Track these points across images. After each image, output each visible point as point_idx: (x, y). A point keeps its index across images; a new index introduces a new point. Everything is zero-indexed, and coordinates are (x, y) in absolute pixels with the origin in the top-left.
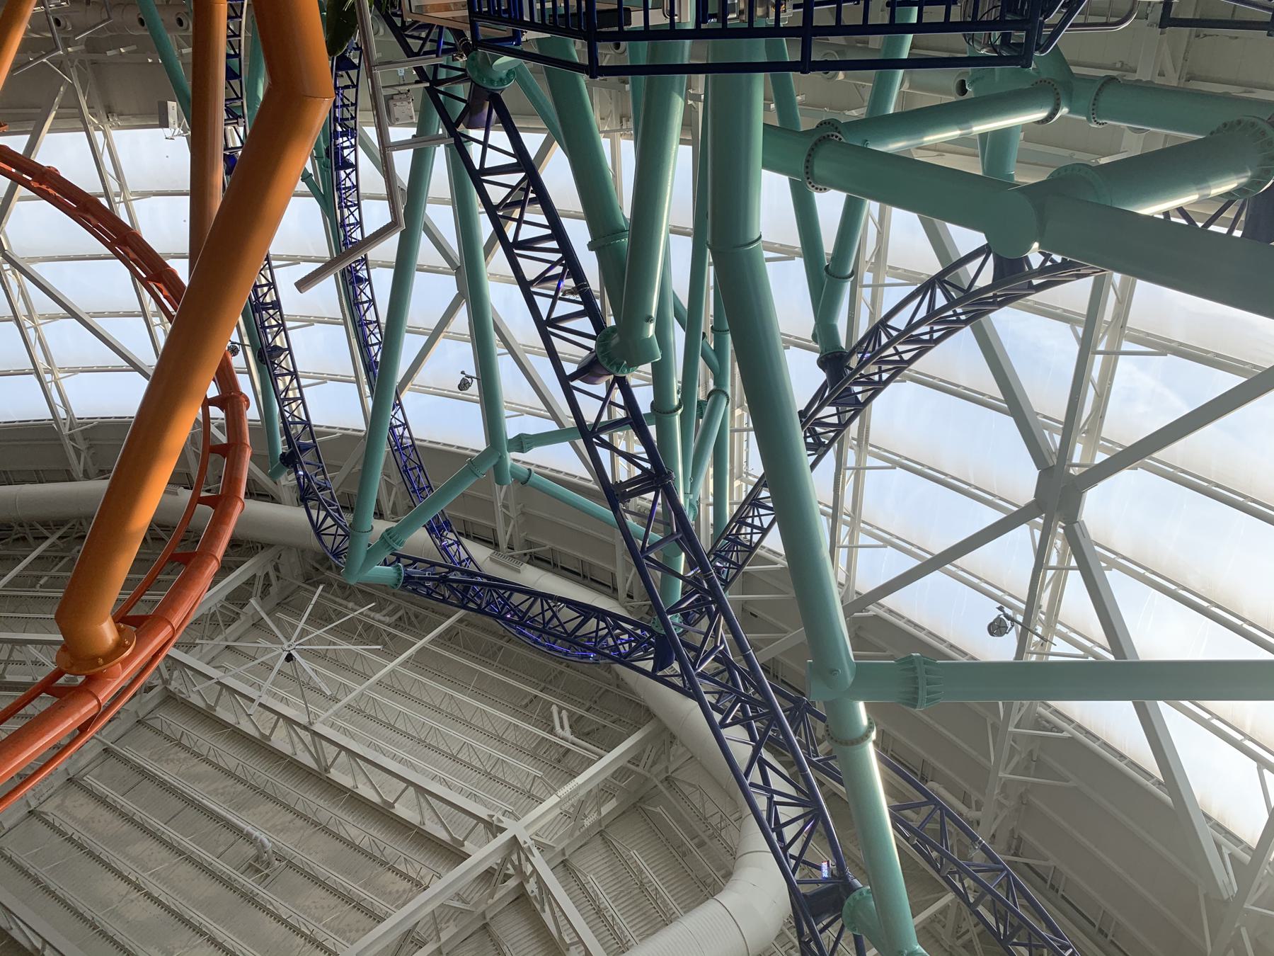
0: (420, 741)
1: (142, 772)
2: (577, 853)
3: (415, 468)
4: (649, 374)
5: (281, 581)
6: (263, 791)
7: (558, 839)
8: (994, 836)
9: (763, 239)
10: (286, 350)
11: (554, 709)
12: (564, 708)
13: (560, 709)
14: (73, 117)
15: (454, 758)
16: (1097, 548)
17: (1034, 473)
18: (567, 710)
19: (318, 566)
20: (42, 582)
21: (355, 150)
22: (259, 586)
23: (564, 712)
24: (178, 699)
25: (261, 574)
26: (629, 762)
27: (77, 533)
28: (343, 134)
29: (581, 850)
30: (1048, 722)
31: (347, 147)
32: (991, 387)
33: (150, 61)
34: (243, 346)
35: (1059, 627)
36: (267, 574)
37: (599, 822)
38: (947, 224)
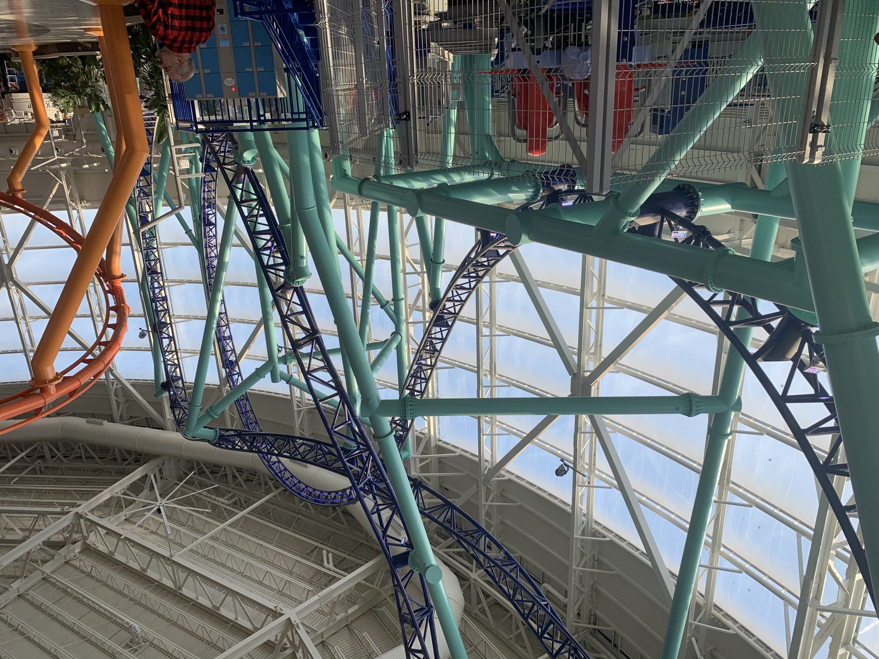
0: (239, 573)
1: (65, 591)
2: (332, 638)
6: (139, 602)
7: (320, 626)
9: (445, 263)
10: (169, 324)
11: (324, 552)
12: (331, 552)
13: (328, 552)
14: (61, 202)
15: (261, 583)
17: (569, 378)
18: (332, 553)
20: (14, 481)
21: (215, 216)
23: (330, 554)
26: (364, 580)
27: (38, 454)
29: (336, 635)
30: (599, 533)
31: (211, 214)
32: (544, 334)
33: (107, 170)
34: (149, 332)
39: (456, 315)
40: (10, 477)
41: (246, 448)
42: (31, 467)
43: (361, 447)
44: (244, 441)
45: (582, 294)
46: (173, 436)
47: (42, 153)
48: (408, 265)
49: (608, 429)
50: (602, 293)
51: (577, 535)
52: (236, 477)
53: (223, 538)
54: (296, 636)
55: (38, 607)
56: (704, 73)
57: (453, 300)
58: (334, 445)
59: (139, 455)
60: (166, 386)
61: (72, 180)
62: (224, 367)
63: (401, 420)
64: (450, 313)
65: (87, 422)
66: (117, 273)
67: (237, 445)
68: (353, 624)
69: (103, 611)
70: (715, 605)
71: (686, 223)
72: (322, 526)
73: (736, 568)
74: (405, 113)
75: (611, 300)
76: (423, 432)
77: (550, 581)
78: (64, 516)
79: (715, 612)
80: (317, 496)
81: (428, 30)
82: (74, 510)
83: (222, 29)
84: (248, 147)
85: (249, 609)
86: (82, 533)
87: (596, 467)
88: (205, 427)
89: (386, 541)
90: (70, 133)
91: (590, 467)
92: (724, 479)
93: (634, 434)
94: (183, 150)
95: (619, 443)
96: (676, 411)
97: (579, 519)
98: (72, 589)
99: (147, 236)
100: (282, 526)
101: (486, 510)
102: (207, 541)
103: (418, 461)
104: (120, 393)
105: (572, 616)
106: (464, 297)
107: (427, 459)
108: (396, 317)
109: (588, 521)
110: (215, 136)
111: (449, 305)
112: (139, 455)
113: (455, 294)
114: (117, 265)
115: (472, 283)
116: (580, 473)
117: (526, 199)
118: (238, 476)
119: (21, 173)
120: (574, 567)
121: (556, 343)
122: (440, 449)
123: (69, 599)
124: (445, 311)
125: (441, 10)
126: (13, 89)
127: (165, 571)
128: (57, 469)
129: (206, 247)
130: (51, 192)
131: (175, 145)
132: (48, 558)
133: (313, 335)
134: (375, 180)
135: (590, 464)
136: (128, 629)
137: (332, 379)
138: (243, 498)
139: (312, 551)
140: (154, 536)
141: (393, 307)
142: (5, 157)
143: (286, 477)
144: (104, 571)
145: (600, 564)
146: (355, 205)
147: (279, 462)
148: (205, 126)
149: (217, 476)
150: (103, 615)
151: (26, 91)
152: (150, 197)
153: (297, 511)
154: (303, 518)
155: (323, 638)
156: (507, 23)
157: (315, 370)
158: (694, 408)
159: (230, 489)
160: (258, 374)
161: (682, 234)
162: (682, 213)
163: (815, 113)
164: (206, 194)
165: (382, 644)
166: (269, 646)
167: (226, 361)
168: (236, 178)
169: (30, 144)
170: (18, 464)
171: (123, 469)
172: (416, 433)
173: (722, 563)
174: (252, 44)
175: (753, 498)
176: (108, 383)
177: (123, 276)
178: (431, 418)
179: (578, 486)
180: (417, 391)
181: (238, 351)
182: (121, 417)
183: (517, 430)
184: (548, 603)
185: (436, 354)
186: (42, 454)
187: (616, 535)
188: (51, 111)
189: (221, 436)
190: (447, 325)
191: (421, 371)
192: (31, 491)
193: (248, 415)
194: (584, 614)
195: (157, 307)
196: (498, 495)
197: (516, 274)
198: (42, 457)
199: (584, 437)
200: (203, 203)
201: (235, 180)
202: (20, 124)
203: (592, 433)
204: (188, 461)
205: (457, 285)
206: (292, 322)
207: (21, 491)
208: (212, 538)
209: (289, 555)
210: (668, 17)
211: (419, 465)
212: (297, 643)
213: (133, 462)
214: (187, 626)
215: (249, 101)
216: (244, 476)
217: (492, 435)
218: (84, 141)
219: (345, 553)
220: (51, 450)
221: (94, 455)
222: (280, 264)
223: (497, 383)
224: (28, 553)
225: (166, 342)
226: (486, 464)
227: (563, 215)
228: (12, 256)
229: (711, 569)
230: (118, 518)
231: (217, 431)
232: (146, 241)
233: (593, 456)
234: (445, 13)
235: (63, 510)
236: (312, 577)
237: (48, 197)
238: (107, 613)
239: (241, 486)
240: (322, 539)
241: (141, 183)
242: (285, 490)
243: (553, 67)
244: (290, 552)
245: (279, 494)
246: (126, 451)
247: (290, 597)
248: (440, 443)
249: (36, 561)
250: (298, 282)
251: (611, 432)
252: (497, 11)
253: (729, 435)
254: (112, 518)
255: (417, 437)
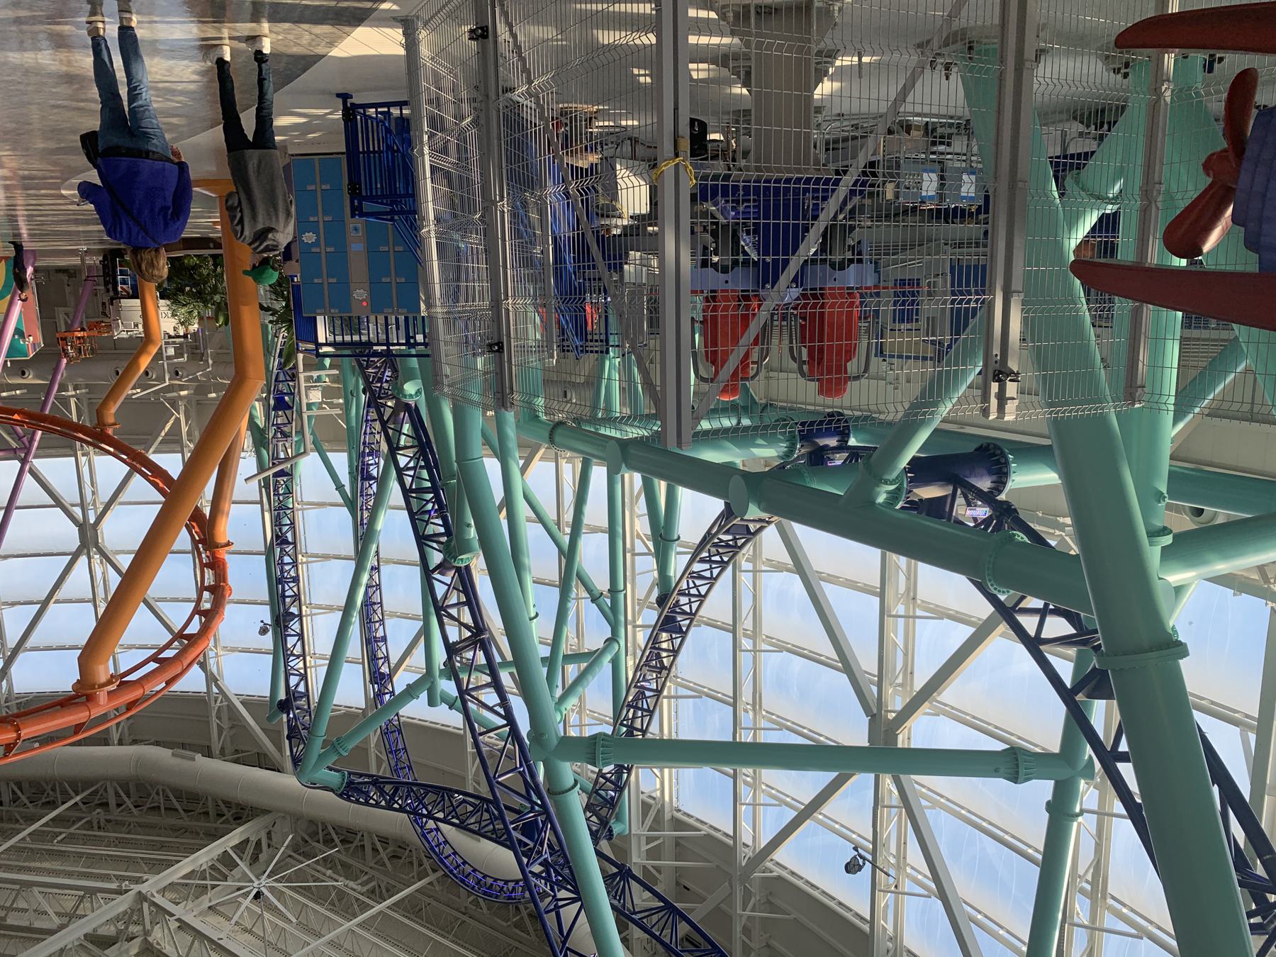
3: (395, 731)
5: (271, 848)
8: (96, 295)
10: (296, 616)
17: (865, 720)
19: (307, 838)
20: (59, 838)
22: (250, 849)
25: (253, 839)
31: (372, 464)
32: (829, 651)
35: (909, 870)
38: (793, 523)
39: (692, 615)
42: (87, 819)
43: (537, 808)
44: (382, 793)
45: (882, 595)
46: (288, 781)
48: (637, 542)
49: (924, 803)
50: (912, 594)
53: (347, 945)
59: (242, 809)
60: (285, 706)
61: (193, 414)
62: (371, 682)
64: (684, 613)
65: (173, 755)
66: (221, 539)
67: (372, 798)
71: (988, 498)
75: (926, 606)
76: (653, 795)
78: (121, 897)
82: (136, 888)
83: (356, 229)
84: (410, 377)
90: (198, 351)
91: (898, 861)
92: (1098, 891)
93: (963, 812)
94: (315, 377)
95: (941, 826)
96: (995, 773)
100: (465, 945)
101: (743, 924)
104: (225, 716)
106: (703, 590)
107: (657, 838)
108: (613, 615)
109: (896, 949)
110: (372, 361)
111: (684, 600)
113: (691, 585)
114: (222, 529)
115: (714, 570)
121: (846, 665)
122: (678, 824)
125: (637, 212)
126: (124, 293)
129: (361, 509)
130: (164, 428)
131: (304, 371)
135: (897, 857)
138: (385, 884)
142: (109, 381)
143: (446, 854)
146: (570, 457)
147: (438, 829)
151: (137, 297)
152: (289, 439)
153: (463, 910)
157: (478, 688)
158: (1022, 771)
159: (366, 869)
160: (411, 692)
161: (982, 512)
163: (999, 358)
167: (375, 673)
168: (393, 417)
171: (216, 829)
172: (641, 796)
177: (229, 544)
178: (666, 771)
181: (394, 660)
185: (665, 672)
188: (167, 321)
189: (351, 783)
190: (680, 631)
191: (642, 698)
192: (80, 855)
193: (400, 755)
195: (283, 591)
198: (105, 805)
199: (889, 814)
200: (362, 449)
201: (392, 419)
203: (901, 807)
204: (310, 821)
205: (694, 572)
207: (67, 854)
208: (331, 943)
210: (953, 223)
211: (645, 848)
213: (231, 819)
215: (397, 319)
216: (390, 849)
217: (754, 805)
218: (210, 362)
221: (177, 805)
222: (441, 535)
223: (763, 724)
225: (291, 641)
226: (746, 850)
227: (808, 480)
230: (200, 904)
231: (344, 775)
233: (901, 844)
235: (120, 886)
239: (384, 865)
241: (279, 419)
242: (445, 875)
245: (437, 879)
246: (224, 802)
248: (679, 815)
250: (462, 559)
252: (578, 229)
253: (1078, 815)
255: (643, 802)
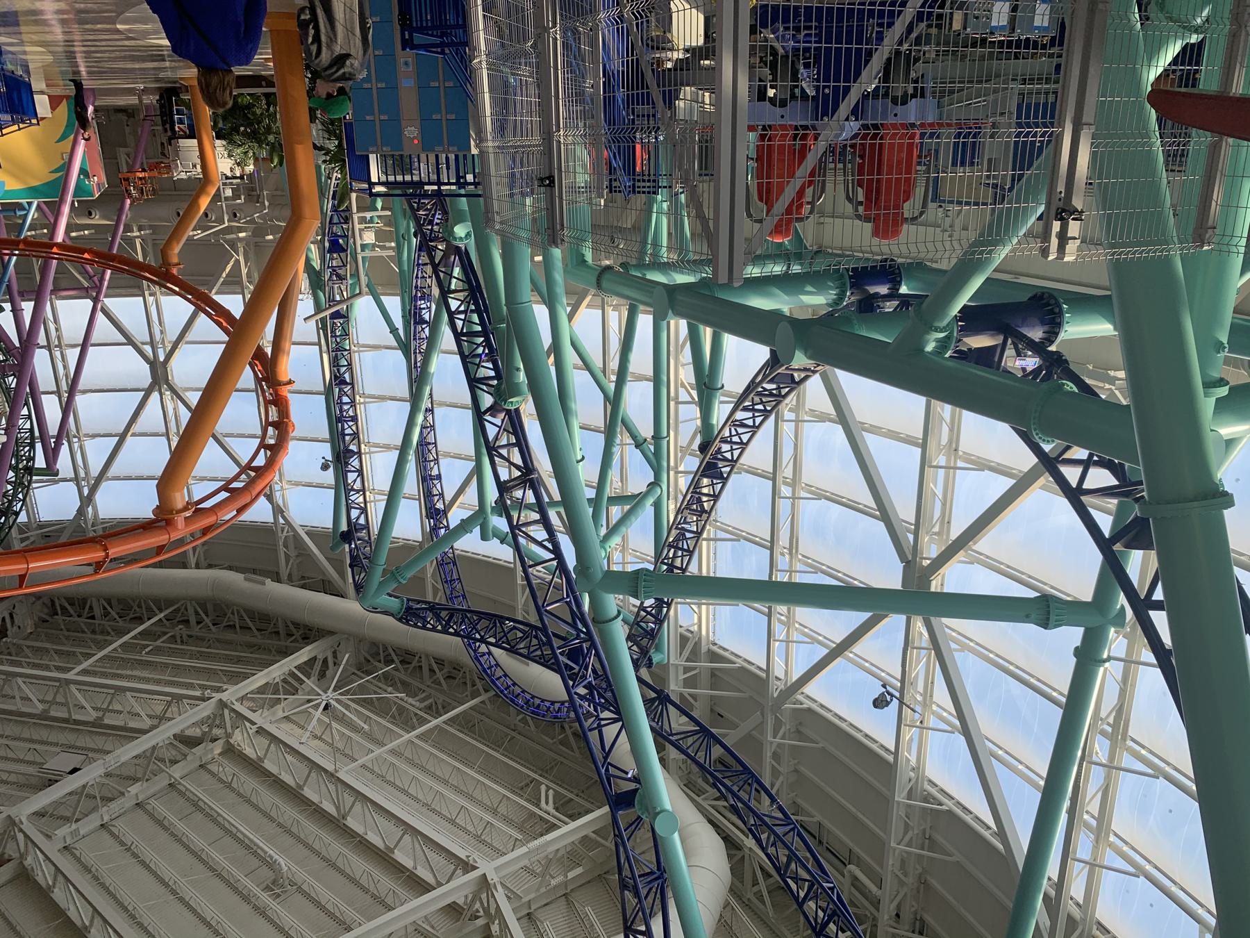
0: (425, 805)
1: (196, 804)
2: (544, 909)
4: (1041, 777)
7: (528, 890)
10: (355, 453)
11: (543, 788)
13: (548, 788)
15: (452, 822)
16: (947, 630)
17: (901, 566)
18: (554, 790)
19: (370, 658)
22: (318, 666)
24: (236, 751)
25: (321, 657)
26: (593, 832)
28: (422, 298)
29: (547, 907)
30: (934, 798)
31: (424, 309)
32: (867, 499)
36: (326, 658)
37: (566, 884)
40: (143, 645)
41: (439, 628)
43: (582, 635)
45: (924, 446)
47: (216, 219)
48: (681, 390)
49: (953, 646)
50: (954, 446)
51: (899, 797)
52: (434, 671)
53: (408, 754)
54: (491, 900)
55: (160, 823)
56: (974, 137)
57: (731, 442)
58: (544, 629)
59: (309, 630)
60: (347, 537)
61: (251, 255)
63: (653, 608)
64: (726, 459)
65: (246, 579)
67: (429, 623)
68: (573, 894)
69: (241, 837)
70: (1099, 923)
71: (1038, 348)
72: (545, 751)
73: (1131, 870)
74: (548, 178)
75: (968, 458)
76: (691, 629)
77: (859, 863)
79: (1098, 933)
80: (516, 693)
81: (675, 69)
82: (217, 696)
83: (406, 64)
85: (432, 856)
86: (225, 728)
87: (934, 700)
88: (390, 595)
89: (607, 770)
90: (254, 193)
91: (925, 699)
92: (1118, 733)
93: (991, 655)
94: (368, 218)
95: (968, 667)
96: (1026, 619)
97: (904, 776)
98: (205, 803)
99: (338, 334)
102: (385, 756)
103: (681, 670)
104: (291, 546)
105: (886, 917)
106: (745, 438)
107: (695, 668)
108: (656, 461)
110: (422, 203)
111: (726, 447)
112: (309, 630)
113: (734, 433)
116: (909, 707)
117: (828, 305)
118: (437, 670)
119: (178, 243)
120: (893, 844)
121: (884, 514)
122: (714, 657)
123: (199, 816)
124: (719, 456)
125: (694, 44)
127: (327, 791)
128: (202, 639)
129: (415, 353)
131: (358, 212)
132: (179, 757)
133: (528, 477)
134: (621, 270)
135: (924, 695)
136: (271, 865)
137: (547, 537)
138: (441, 700)
139: (527, 785)
140: (317, 742)
141: (652, 448)
143: (497, 675)
144: (248, 783)
145: (932, 845)
146: (616, 305)
147: (490, 653)
148: (388, 188)
149: (408, 668)
150: (240, 842)
152: (344, 282)
154: (518, 737)
155: (530, 908)
156: (334, 91)
158: (1053, 618)
159: (423, 687)
160: (465, 526)
161: (1031, 362)
162: (1036, 334)
163: (1063, 195)
164: (419, 281)
165: (609, 924)
166: (453, 910)
167: (431, 508)
169: (194, 204)
170: (154, 628)
173: (1111, 858)
174: (441, 84)
175: (1162, 765)
176: (276, 527)
177: (290, 382)
179: (905, 725)
180: (677, 568)
182: (290, 576)
183: (825, 638)
184: (835, 886)
185: (705, 516)
186: (186, 618)
187: (959, 803)
188: (224, 163)
189: (409, 609)
192: (166, 665)
193: (454, 585)
194: (907, 916)
195: (343, 429)
196: (792, 730)
197: (831, 410)
198: (186, 622)
199: (918, 655)
201: (443, 262)
202: (190, 178)
203: (930, 649)
205: (736, 421)
206: (501, 456)
208: (393, 752)
209: (495, 786)
211: (682, 677)
212: (493, 911)
214: (348, 871)
216: (445, 670)
217: (788, 642)
218: (267, 203)
219: (572, 792)
220: (197, 613)
221: (251, 624)
223: (799, 567)
224: (154, 748)
225: (351, 477)
226: (778, 683)
228: (170, 351)
229: (1094, 866)
231: (403, 601)
232: (336, 340)
233: (929, 684)
234: (700, 48)
235: (203, 694)
236: (524, 822)
237: (220, 276)
238: (246, 841)
240: (542, 770)
241: (334, 262)
242: (496, 695)
243: (809, 123)
244: (496, 782)
246: (293, 623)
247: (490, 846)
248: (715, 648)
249: (163, 760)
250: (512, 402)
251: (956, 650)
252: (632, 55)
253: (1105, 661)
254: (266, 713)
255: (682, 636)
